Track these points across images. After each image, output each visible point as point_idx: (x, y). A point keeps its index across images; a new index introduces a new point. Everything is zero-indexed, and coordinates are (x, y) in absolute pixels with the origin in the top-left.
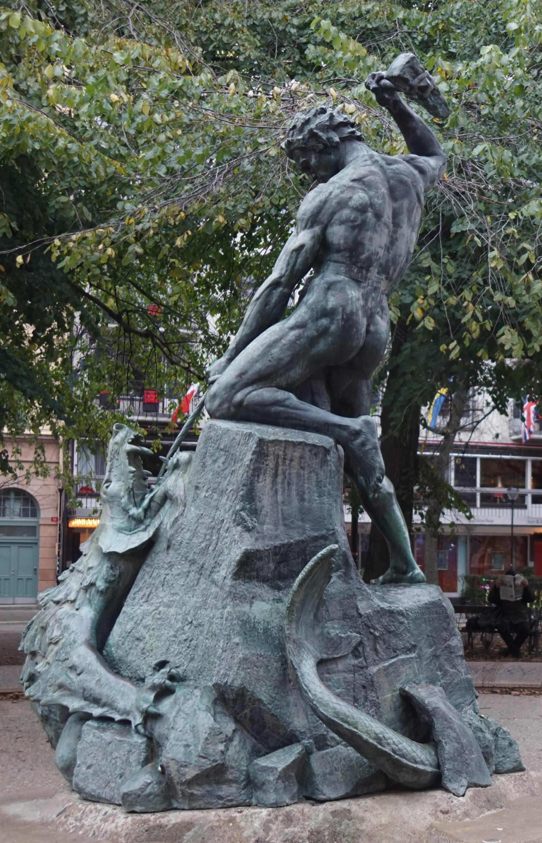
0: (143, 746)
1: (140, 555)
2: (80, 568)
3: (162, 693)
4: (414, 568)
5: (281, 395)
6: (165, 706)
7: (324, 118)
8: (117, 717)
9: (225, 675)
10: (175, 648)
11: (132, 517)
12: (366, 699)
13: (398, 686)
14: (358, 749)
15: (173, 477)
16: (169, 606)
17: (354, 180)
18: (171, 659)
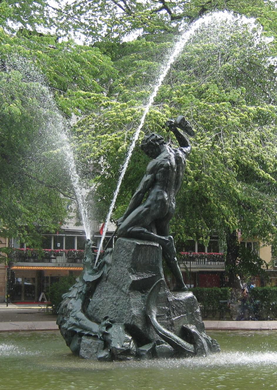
0: (103, 343)
1: (96, 283)
2: (76, 286)
3: (108, 326)
4: (184, 286)
5: (143, 229)
6: (110, 331)
7: (154, 137)
8: (93, 335)
9: (128, 321)
10: (110, 312)
11: (94, 270)
12: (171, 329)
13: (181, 325)
14: (171, 345)
15: (107, 257)
16: (107, 299)
17: (165, 158)
18: (109, 316)
